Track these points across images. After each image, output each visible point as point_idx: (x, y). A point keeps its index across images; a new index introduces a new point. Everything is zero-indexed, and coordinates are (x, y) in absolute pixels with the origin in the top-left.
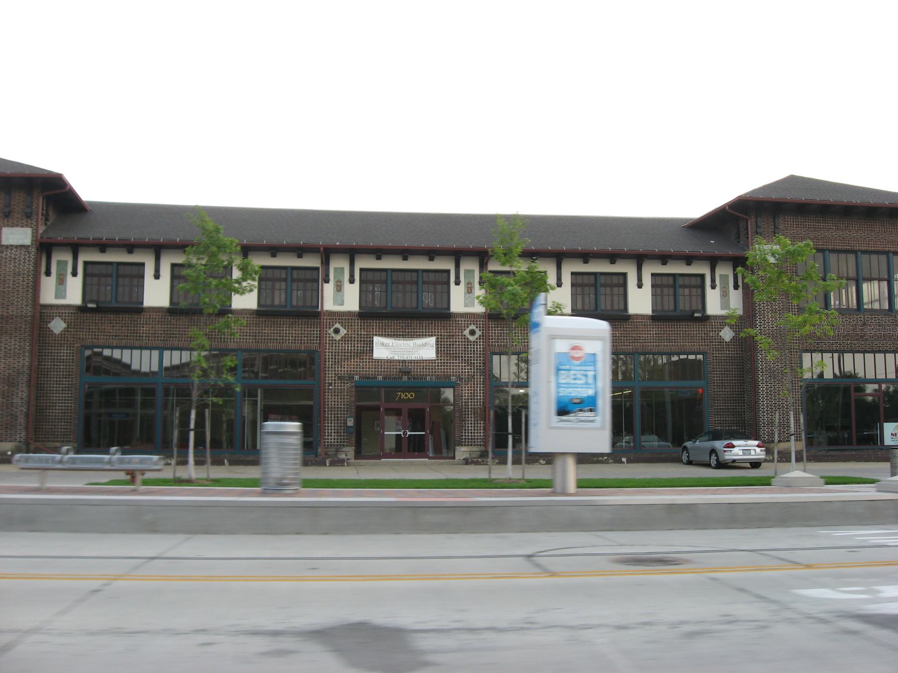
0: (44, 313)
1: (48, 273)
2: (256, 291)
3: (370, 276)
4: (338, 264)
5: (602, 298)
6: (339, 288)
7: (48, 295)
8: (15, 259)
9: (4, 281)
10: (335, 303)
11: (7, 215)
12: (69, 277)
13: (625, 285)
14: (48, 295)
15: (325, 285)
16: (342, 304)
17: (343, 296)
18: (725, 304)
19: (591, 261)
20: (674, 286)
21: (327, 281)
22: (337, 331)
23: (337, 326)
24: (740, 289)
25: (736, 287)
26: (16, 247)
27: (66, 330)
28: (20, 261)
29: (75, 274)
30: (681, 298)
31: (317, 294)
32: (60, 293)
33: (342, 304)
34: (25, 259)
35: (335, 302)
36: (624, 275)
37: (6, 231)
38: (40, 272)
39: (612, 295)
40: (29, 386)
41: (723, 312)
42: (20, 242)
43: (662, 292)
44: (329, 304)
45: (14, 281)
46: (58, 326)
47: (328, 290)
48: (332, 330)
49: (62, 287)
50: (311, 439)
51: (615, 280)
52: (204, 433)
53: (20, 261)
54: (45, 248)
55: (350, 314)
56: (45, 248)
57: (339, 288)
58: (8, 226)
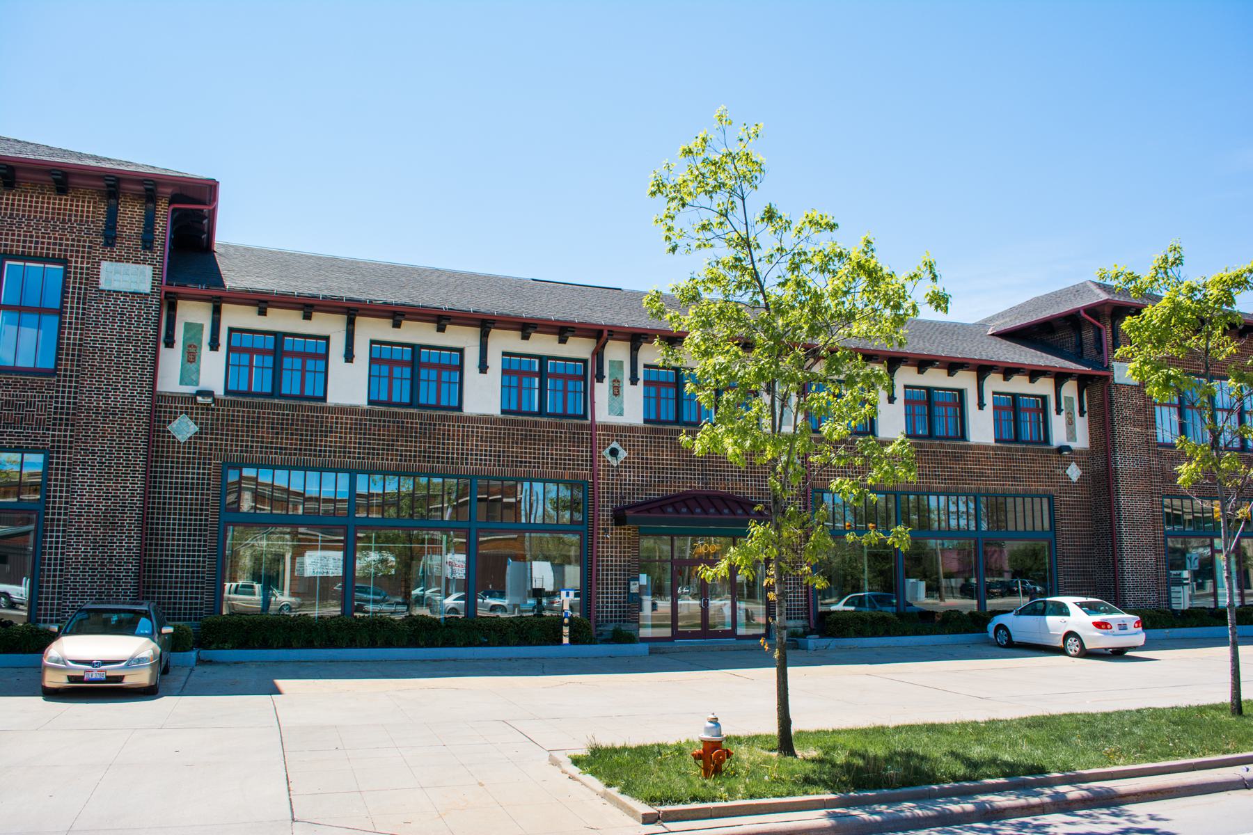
0: (161, 408)
1: (170, 343)
3: (247, 341)
4: (617, 352)
5: (423, 385)
6: (616, 391)
7: (170, 380)
8: (122, 314)
9: (102, 350)
10: (611, 411)
11: (110, 237)
12: (205, 348)
13: (460, 368)
14: (170, 380)
15: (597, 385)
16: (202, 326)
17: (622, 402)
18: (1072, 435)
19: (1016, 378)
20: (542, 374)
21: (600, 378)
22: (614, 453)
23: (615, 445)
24: (641, 383)
25: (1082, 414)
26: (126, 294)
27: (197, 436)
28: (130, 318)
29: (214, 346)
30: (685, 403)
31: (588, 397)
32: (1072, 435)
33: (202, 326)
34: (139, 316)
35: (611, 411)
36: (461, 351)
39: (391, 377)
41: (190, 390)
42: (133, 288)
43: (304, 365)
44: (603, 415)
45: (119, 351)
46: (183, 428)
47: (602, 391)
48: (607, 451)
49: (193, 366)
50: (566, 640)
51: (311, 345)
55: (632, 429)
57: (616, 391)
58: (111, 259)
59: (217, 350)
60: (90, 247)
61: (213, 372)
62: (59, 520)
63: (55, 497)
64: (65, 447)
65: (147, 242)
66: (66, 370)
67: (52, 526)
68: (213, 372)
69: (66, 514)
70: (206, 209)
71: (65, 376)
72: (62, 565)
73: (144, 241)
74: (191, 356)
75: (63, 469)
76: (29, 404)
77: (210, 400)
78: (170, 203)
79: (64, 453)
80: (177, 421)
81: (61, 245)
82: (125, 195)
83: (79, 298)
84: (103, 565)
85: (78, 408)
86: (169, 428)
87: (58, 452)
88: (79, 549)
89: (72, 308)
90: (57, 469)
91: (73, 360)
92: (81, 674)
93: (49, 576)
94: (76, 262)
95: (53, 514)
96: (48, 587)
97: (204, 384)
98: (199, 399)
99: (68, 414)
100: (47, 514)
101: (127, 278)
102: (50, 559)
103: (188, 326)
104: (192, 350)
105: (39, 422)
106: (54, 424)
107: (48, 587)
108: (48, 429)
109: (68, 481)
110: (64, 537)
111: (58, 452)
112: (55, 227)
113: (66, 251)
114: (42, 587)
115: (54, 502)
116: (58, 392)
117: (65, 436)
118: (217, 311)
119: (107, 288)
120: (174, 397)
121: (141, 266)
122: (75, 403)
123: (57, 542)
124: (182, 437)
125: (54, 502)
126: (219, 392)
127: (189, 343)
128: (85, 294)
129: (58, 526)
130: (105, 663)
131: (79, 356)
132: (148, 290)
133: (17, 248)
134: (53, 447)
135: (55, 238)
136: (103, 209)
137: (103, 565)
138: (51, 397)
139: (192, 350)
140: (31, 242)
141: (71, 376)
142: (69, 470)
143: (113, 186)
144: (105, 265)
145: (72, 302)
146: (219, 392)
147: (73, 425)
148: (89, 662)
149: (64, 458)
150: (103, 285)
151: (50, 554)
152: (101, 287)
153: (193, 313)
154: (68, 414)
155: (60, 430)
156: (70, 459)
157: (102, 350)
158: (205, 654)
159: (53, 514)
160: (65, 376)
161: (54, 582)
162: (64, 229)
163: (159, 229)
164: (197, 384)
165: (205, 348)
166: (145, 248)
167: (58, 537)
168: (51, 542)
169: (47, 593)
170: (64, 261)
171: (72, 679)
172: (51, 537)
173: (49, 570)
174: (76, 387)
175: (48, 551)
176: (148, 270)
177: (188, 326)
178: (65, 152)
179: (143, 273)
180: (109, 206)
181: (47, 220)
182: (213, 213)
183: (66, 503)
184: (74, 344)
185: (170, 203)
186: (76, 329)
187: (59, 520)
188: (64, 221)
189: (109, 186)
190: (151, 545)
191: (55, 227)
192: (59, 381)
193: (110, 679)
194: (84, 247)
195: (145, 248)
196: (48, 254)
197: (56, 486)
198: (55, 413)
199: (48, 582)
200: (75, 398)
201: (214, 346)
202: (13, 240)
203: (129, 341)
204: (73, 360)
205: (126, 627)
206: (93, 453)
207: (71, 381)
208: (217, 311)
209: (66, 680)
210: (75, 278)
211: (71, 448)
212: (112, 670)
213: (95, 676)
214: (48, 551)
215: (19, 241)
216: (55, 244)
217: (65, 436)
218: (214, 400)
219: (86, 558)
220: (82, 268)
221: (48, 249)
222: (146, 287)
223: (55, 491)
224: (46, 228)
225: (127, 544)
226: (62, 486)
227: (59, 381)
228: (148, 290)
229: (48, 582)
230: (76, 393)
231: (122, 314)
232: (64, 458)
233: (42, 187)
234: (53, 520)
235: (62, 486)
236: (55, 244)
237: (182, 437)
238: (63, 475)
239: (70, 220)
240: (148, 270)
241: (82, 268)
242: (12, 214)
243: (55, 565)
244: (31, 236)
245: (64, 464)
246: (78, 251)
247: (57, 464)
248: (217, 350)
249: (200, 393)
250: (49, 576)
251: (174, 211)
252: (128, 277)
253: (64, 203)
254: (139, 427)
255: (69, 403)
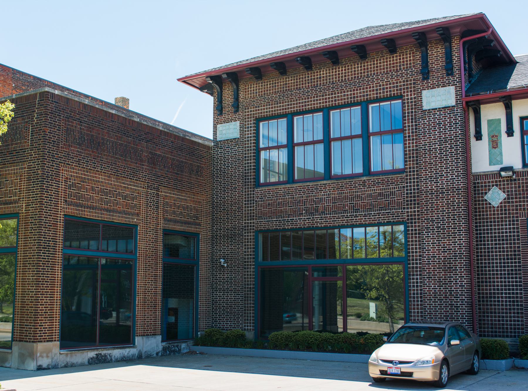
0: (475, 185)
1: (479, 136)
2: (114, 103)
7: (481, 161)
8: (439, 124)
9: (430, 150)
11: (426, 73)
14: (481, 161)
16: (499, 120)
26: (440, 109)
27: (506, 201)
28: (445, 125)
29: (510, 133)
33: (499, 120)
34: (450, 122)
37: (426, 94)
38: (469, 136)
40: (470, 272)
41: (496, 168)
42: (444, 104)
45: (441, 149)
46: (496, 197)
49: (496, 150)
52: (112, 109)
53: (445, 125)
54: (472, 106)
56: (472, 106)
58: (428, 88)
59: (512, 135)
60: (414, 83)
61: (511, 153)
62: (417, 268)
63: (413, 252)
64: (415, 219)
65: (449, 70)
66: (410, 168)
67: (413, 272)
68: (511, 153)
69: (420, 263)
70: (486, 35)
71: (410, 172)
72: (421, 297)
73: (447, 70)
74: (495, 143)
75: (416, 234)
76: (392, 193)
77: (511, 173)
78: (462, 38)
79: (415, 223)
80: (491, 192)
81: (397, 87)
82: (431, 43)
83: (412, 119)
84: (446, 297)
85: (420, 191)
86: (485, 198)
87: (411, 223)
88: (431, 286)
89: (409, 126)
90: (412, 234)
91: (413, 161)
92: (385, 369)
93: (414, 305)
94: (407, 95)
95: (413, 263)
96: (414, 312)
97: (506, 163)
98: (503, 174)
99: (414, 197)
100: (409, 264)
101: (439, 98)
102: (414, 294)
103: (490, 122)
104: (495, 139)
105: (398, 204)
106: (408, 205)
107: (414, 312)
108: (404, 208)
109: (419, 241)
110: (421, 279)
111: (411, 223)
112: (392, 75)
113: (401, 90)
114: (411, 312)
115: (413, 256)
116: (407, 183)
117: (415, 211)
118: (508, 108)
119: (428, 108)
120: (486, 175)
121: (447, 88)
122: (418, 189)
123: (417, 283)
124: (495, 203)
125: (413, 256)
126: (518, 165)
127: (492, 134)
128: (415, 115)
129: (417, 271)
130: (401, 362)
131: (417, 157)
132: (454, 104)
133: (373, 96)
134: (408, 219)
135: (394, 83)
136: (418, 55)
137: (446, 297)
138: (404, 187)
139: (495, 139)
140: (380, 89)
141: (414, 171)
142: (419, 234)
143: (421, 38)
144: (424, 93)
145: (408, 123)
146: (518, 165)
147: (418, 204)
148: (391, 362)
149: (415, 226)
150: (426, 107)
151: (414, 290)
152: (424, 108)
153: (492, 112)
154: (414, 197)
155: (411, 208)
156: (419, 226)
157: (430, 150)
158: (519, 362)
159: (413, 263)
160: (410, 172)
161: (418, 309)
162: (397, 76)
163: (455, 59)
164: (502, 163)
165: (504, 135)
166: (448, 75)
167: (417, 279)
168: (414, 283)
169: (414, 316)
170: (400, 97)
171: (383, 372)
172: (413, 279)
173: (414, 301)
174: (417, 178)
175: (412, 288)
176: (452, 89)
177: (490, 122)
178: (402, 25)
179: (449, 92)
180: (422, 52)
181: (387, 73)
182: (494, 34)
183: (420, 256)
184: (413, 150)
185: (462, 38)
186: (413, 139)
187: (417, 268)
188: (397, 71)
189: (441, 34)
190: (482, 282)
191: (392, 75)
192: (407, 176)
193: (403, 374)
194: (411, 84)
195: (448, 75)
196: (390, 94)
197: (412, 245)
198: (407, 197)
199: (414, 309)
200: (418, 185)
201: (510, 133)
202: (370, 91)
203: (446, 142)
204: (413, 161)
205: (425, 341)
206: (433, 221)
207: (414, 175)
208: (508, 108)
209: (379, 373)
210: (408, 106)
211: (419, 219)
212: (405, 368)
213: (394, 371)
214: (412, 288)
215: (373, 91)
216: (394, 87)
217: (415, 211)
218: (514, 173)
219: (435, 293)
220: (411, 99)
221: (390, 91)
222: (452, 102)
223: (413, 249)
224: (387, 78)
225: (460, 281)
226: (416, 245)
227: (407, 176)
228: (454, 104)
229: (414, 309)
230: (417, 182)
231: (439, 124)
232: (415, 226)
233: (382, 53)
234: (413, 268)
235: (416, 245)
236: (394, 87)
237: (495, 203)
238: (416, 237)
239: (400, 69)
240: (452, 89)
241: (411, 99)
242: (368, 75)
243: (417, 297)
244: (380, 86)
245: (416, 230)
246: (407, 88)
247: (412, 230)
248: (512, 135)
249: (504, 169)
250: (414, 305)
251: (464, 43)
252: (440, 97)
253: (396, 59)
254: (459, 199)
255: (414, 189)
